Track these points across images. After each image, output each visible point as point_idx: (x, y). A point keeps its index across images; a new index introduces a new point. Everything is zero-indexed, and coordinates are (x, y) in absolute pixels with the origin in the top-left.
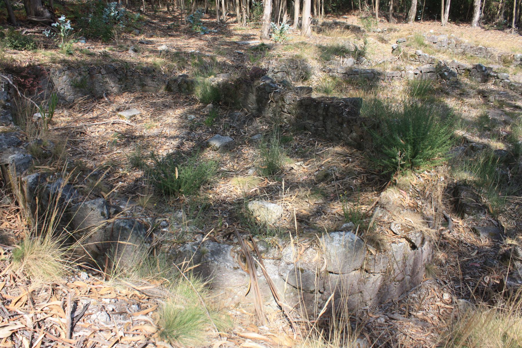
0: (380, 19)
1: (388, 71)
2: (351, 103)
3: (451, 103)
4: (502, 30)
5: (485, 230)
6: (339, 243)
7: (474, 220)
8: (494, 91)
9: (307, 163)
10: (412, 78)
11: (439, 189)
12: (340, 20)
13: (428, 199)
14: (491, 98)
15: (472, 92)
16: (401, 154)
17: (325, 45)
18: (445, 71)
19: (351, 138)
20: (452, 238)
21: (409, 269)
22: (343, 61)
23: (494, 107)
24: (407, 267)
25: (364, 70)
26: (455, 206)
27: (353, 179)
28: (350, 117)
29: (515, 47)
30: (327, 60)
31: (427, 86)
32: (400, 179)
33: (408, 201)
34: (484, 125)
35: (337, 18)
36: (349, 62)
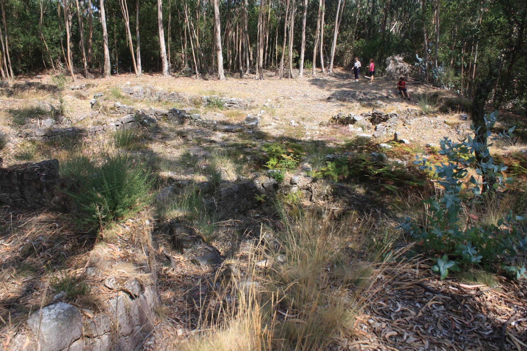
0: (76, 76)
1: (90, 126)
2: (46, 166)
3: (156, 147)
4: (190, 76)
5: (203, 258)
6: (49, 319)
7: (192, 252)
8: (191, 130)
9: (9, 240)
10: (115, 130)
11: (146, 233)
12: (35, 80)
13: (137, 245)
14: (189, 137)
15: (173, 134)
16: (100, 208)
17: (17, 109)
18: (145, 119)
19: (54, 202)
20: (177, 274)
21: (136, 320)
22: (41, 124)
23: (193, 145)
24: (133, 318)
25: (64, 129)
26: (173, 243)
27: (63, 244)
28: (48, 181)
29: (201, 90)
30: (22, 124)
31: (130, 135)
32: (106, 233)
33: (118, 252)
34: (188, 163)
35: (30, 79)
36: (48, 123)
